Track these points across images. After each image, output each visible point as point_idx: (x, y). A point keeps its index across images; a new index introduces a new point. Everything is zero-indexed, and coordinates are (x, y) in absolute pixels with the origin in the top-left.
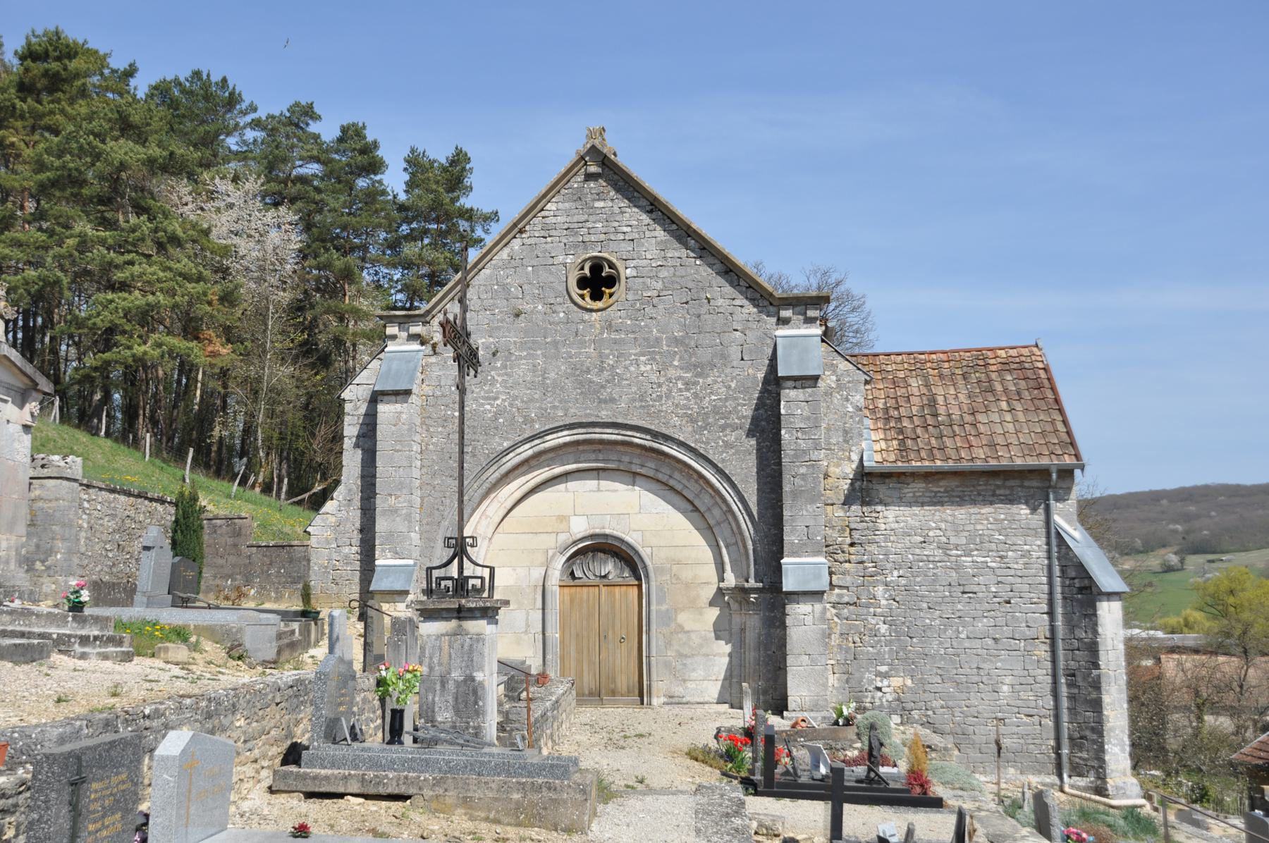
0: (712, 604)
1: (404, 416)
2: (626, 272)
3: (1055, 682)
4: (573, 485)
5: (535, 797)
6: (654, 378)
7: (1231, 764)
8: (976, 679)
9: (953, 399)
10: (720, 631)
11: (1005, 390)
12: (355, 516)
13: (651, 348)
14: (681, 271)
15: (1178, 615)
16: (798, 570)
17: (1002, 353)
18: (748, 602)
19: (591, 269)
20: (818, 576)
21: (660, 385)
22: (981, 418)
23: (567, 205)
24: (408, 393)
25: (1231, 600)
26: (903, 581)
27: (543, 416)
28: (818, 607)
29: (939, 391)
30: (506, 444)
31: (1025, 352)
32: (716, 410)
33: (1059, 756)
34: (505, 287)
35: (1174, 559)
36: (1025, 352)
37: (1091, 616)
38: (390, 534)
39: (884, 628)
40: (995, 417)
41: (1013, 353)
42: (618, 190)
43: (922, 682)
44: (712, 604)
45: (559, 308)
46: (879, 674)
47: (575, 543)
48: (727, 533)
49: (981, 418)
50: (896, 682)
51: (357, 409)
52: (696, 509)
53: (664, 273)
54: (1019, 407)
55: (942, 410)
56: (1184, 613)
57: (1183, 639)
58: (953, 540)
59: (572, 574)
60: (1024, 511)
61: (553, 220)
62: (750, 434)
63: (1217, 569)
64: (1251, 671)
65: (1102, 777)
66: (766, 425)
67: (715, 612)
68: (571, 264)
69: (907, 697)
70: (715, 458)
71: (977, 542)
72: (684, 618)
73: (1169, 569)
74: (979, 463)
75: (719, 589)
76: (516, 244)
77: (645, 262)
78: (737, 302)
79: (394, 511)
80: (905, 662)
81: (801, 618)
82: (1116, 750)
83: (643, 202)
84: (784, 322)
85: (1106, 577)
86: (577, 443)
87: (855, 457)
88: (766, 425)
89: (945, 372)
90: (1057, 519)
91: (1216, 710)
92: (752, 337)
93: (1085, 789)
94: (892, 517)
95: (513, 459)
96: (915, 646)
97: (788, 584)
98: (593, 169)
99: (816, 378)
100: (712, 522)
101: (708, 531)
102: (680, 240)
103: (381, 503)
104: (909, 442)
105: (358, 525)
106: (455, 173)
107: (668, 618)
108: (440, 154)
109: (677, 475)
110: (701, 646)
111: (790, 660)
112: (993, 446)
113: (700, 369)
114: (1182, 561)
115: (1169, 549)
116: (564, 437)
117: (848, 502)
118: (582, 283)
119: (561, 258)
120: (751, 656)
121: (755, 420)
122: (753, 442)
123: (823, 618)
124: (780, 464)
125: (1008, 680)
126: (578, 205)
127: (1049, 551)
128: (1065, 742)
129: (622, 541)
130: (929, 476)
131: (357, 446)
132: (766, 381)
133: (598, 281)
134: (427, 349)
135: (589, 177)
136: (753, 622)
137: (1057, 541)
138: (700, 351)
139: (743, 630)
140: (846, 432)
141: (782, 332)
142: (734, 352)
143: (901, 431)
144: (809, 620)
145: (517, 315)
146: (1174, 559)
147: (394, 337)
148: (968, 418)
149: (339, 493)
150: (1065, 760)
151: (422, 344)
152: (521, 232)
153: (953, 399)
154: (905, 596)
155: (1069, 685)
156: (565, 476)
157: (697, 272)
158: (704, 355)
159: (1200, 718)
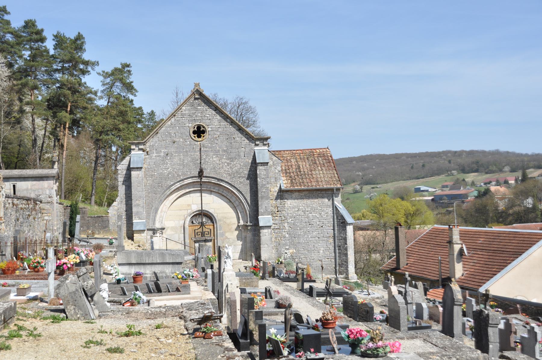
0: (236, 230)
1: (140, 175)
2: (208, 129)
3: (335, 249)
4: (192, 195)
5: (248, 281)
6: (218, 162)
7: (380, 270)
8: (313, 249)
9: (305, 166)
10: (239, 238)
11: (320, 163)
12: (123, 207)
13: (216, 153)
14: (225, 129)
15: (360, 212)
16: (263, 220)
17: (318, 151)
18: (247, 229)
19: (197, 128)
20: (269, 221)
21: (220, 164)
22: (313, 172)
23: (189, 108)
24: (141, 168)
25: (381, 208)
26: (292, 222)
27: (184, 174)
28: (270, 230)
29: (300, 163)
30: (172, 183)
31: (325, 150)
32: (237, 172)
33: (336, 269)
34: (170, 133)
35: (358, 187)
36: (325, 150)
37: (345, 230)
38: (138, 213)
39: (287, 236)
40: (317, 172)
41: (321, 150)
42: (205, 103)
43: (298, 250)
44: (236, 230)
45: (187, 140)
46: (286, 249)
47: (193, 213)
48: (240, 208)
49: (313, 172)
50: (291, 251)
51: (122, 172)
52: (231, 202)
53: (220, 130)
54: (324, 169)
55: (302, 170)
56: (362, 211)
57: (361, 223)
58: (307, 209)
59: (192, 222)
60: (326, 200)
61: (184, 112)
62: (247, 179)
63: (376, 191)
64: (387, 238)
65: (347, 274)
66: (253, 177)
67: (237, 232)
68: (191, 126)
69: (294, 255)
70: (237, 187)
71: (313, 210)
72: (227, 234)
73: (356, 192)
74: (314, 187)
75: (238, 225)
76: (173, 120)
77: (214, 126)
78: (243, 139)
79: (138, 205)
80: (293, 245)
81: (265, 234)
82: (351, 267)
83: (213, 107)
84: (257, 145)
85: (349, 219)
86: (194, 182)
87: (278, 186)
88: (253, 177)
89: (302, 157)
90: (335, 202)
91: (375, 251)
92: (247, 150)
93: (343, 278)
94: (289, 203)
95: (174, 188)
96: (296, 240)
97: (261, 224)
98: (197, 96)
99: (268, 163)
100: (236, 205)
101: (235, 208)
102: (225, 119)
103: (134, 203)
104: (293, 181)
105: (125, 209)
106: (78, 43)
107: (223, 234)
108: (71, 35)
109: (225, 191)
110: (233, 243)
111: (262, 246)
112: (317, 181)
113: (232, 159)
114: (361, 188)
115: (356, 183)
116: (190, 180)
117: (276, 199)
118: (194, 132)
119: (187, 125)
120: (248, 245)
121: (249, 175)
122: (248, 181)
123: (271, 234)
124: (257, 188)
125: (322, 249)
126: (192, 107)
127: (333, 212)
128: (338, 265)
129: (208, 212)
130: (299, 191)
131: (123, 184)
132: (252, 163)
133: (199, 132)
134: (145, 153)
135: (195, 99)
136: (249, 235)
137: (335, 209)
138: (232, 154)
139: (246, 237)
140: (276, 178)
141: (256, 148)
142: (242, 154)
143: (291, 177)
144: (267, 234)
145: (174, 143)
146: (358, 187)
147: (134, 149)
148: (310, 173)
149: (118, 199)
150: (337, 270)
151: (143, 151)
152: (174, 116)
153: (305, 166)
154: (293, 226)
155: (339, 250)
156: (190, 192)
157: (230, 129)
158: (233, 155)
159: (370, 256)
